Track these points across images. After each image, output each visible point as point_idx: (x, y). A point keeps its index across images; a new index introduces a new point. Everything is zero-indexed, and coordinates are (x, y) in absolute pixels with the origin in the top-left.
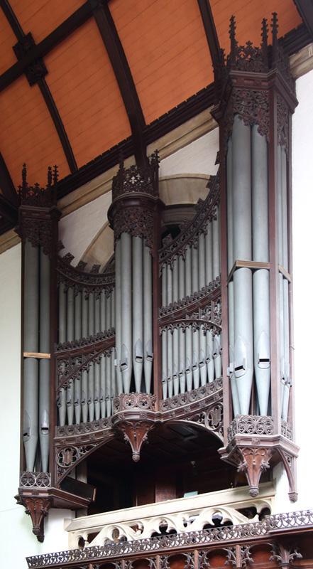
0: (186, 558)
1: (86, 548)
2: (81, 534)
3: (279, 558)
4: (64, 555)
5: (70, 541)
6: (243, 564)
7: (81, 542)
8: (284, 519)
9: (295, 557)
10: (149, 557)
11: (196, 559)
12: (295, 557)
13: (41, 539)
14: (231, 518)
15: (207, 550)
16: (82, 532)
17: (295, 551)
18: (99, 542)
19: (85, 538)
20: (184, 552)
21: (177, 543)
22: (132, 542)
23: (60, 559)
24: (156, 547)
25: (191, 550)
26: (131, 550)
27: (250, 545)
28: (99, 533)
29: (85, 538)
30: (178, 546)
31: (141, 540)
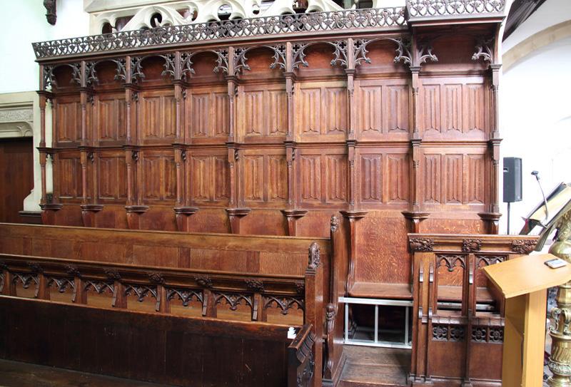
0: (164, 61)
1: (123, 33)
2: (107, 18)
3: (407, 60)
4: (77, 43)
5: (91, 26)
6: (183, 76)
7: (107, 28)
8: (431, 3)
9: (428, 59)
10: (72, 63)
11: (289, 55)
12: (428, 59)
13: (52, 19)
14: (241, 12)
15: (96, 61)
16: (109, 15)
17: (429, 52)
18: (133, 26)
19: (113, 24)
20: (113, 58)
21: (247, 32)
22: (180, 27)
23: (83, 47)
24: (291, 31)
25: (122, 55)
26: (177, 38)
27: (367, 39)
28: (133, 16)
29: (113, 24)
30: (93, 51)
31: (50, 42)
